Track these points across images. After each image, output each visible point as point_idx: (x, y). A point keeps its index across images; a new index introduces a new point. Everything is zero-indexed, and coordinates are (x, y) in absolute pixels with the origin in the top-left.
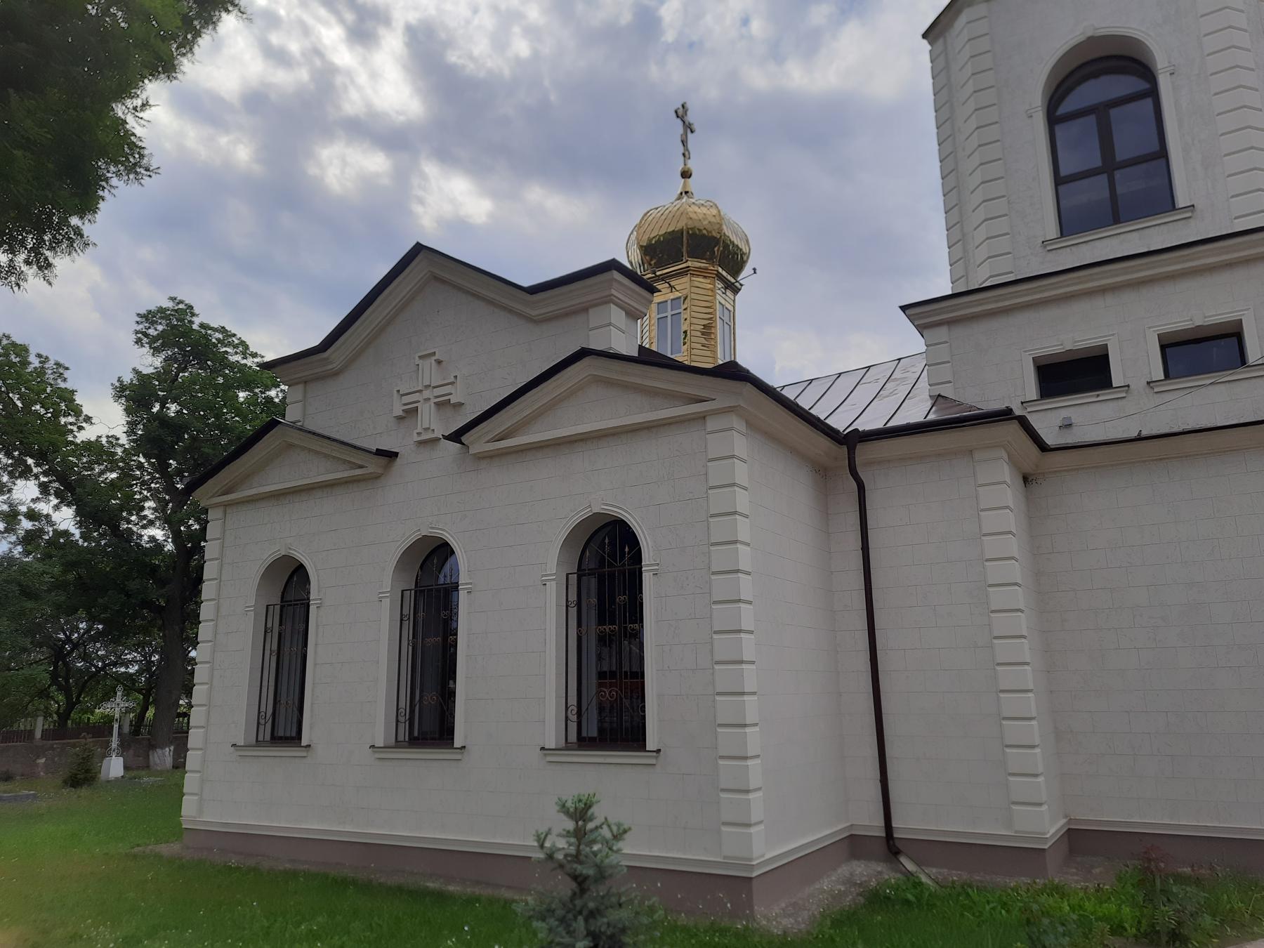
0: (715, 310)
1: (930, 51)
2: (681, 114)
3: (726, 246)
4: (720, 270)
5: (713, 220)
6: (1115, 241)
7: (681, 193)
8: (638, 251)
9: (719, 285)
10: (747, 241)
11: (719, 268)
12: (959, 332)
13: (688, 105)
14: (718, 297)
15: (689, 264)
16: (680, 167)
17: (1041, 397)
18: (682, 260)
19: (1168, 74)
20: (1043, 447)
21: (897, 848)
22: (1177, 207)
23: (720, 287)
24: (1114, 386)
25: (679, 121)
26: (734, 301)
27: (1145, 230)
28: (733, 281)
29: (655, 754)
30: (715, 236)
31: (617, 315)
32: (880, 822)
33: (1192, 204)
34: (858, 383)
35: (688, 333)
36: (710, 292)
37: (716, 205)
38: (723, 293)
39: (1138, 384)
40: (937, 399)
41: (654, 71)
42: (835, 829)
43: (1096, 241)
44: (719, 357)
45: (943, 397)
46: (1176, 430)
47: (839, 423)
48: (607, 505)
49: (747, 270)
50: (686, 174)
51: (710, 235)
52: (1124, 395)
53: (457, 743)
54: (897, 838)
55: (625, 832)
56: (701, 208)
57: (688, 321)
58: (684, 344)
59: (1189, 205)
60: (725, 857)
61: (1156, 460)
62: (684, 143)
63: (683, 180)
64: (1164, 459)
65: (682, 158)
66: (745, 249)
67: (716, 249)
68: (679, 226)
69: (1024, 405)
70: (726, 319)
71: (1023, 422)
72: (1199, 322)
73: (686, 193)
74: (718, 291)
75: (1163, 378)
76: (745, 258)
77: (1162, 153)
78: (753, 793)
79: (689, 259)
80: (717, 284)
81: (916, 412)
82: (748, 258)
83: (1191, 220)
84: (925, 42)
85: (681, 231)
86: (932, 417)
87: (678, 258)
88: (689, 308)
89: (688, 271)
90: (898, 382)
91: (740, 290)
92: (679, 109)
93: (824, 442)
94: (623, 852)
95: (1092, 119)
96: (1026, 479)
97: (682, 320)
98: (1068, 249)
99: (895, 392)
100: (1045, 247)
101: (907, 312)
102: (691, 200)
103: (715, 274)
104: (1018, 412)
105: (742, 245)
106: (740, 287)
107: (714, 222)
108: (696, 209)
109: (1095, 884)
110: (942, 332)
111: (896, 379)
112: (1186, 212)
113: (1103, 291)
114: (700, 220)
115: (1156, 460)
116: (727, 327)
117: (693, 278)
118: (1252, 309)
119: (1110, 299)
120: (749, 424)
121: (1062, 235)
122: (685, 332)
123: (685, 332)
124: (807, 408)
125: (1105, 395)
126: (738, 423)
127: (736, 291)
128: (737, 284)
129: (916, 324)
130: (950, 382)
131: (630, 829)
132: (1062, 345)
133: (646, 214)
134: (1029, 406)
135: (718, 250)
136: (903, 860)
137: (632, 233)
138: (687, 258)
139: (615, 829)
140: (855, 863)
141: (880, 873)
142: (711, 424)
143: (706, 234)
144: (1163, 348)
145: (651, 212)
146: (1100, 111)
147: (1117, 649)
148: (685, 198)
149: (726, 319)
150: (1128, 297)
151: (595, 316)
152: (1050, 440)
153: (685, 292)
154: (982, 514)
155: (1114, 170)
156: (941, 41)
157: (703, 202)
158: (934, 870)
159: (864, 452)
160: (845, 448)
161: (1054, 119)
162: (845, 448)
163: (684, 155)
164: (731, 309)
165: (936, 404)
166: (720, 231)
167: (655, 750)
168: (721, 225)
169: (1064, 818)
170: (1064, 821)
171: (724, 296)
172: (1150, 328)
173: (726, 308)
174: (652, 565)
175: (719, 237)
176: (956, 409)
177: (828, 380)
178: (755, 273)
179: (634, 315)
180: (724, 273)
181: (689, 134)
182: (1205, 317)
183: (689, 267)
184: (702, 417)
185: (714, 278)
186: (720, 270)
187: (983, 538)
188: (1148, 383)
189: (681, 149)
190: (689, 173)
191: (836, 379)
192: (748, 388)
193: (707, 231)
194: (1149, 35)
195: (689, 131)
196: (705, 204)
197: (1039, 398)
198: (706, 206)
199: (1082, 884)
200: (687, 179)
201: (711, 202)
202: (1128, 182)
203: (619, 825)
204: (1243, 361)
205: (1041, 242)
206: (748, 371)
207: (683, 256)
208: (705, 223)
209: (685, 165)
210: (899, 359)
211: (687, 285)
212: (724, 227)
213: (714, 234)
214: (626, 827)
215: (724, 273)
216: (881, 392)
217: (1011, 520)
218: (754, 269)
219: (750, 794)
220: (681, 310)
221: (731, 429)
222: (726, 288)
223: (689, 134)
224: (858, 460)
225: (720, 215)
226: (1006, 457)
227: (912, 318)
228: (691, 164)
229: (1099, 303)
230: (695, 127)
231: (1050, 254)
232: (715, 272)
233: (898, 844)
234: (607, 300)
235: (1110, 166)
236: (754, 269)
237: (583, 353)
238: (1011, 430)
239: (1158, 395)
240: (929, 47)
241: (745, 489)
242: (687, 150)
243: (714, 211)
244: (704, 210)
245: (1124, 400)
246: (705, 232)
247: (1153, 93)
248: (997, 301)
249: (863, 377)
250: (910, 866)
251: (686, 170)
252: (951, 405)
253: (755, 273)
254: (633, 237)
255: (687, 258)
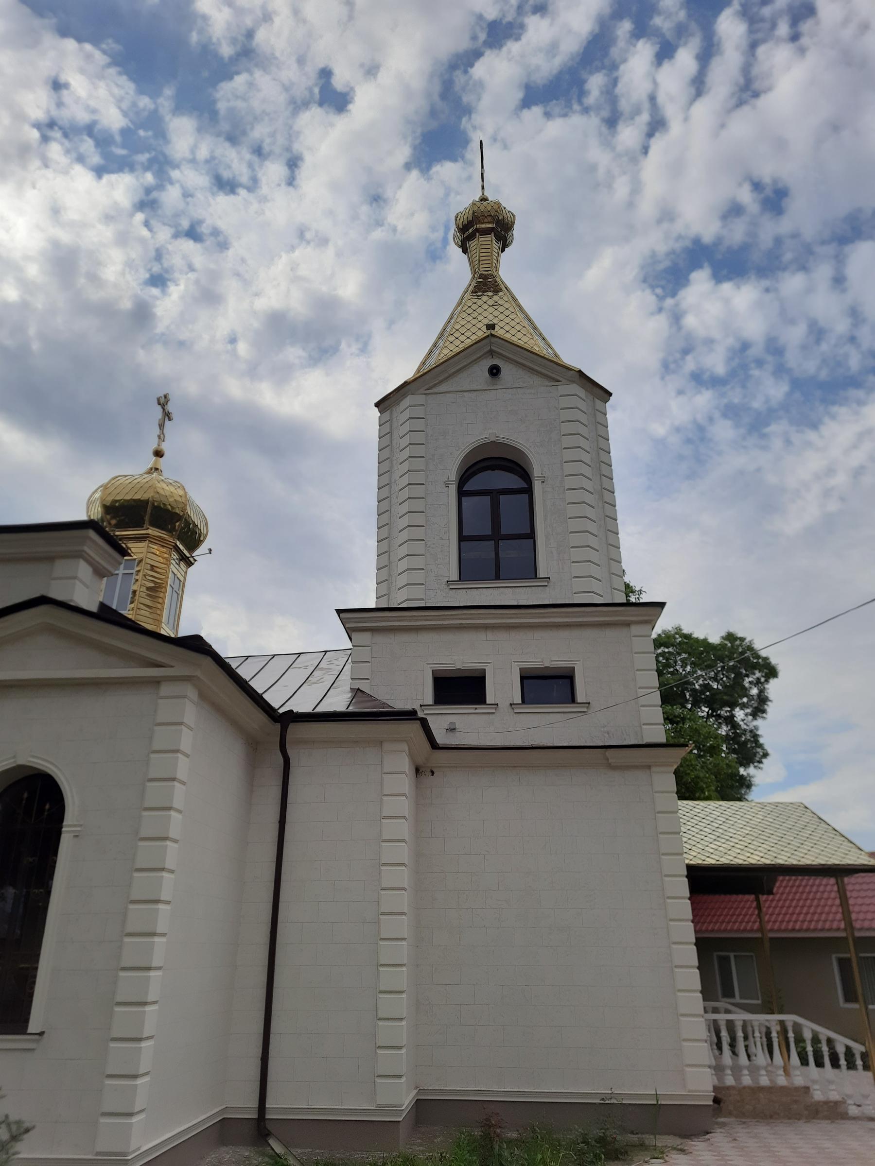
0: (168, 578)
1: (379, 417)
2: (163, 402)
3: (187, 523)
4: (178, 543)
5: (179, 499)
6: (496, 592)
7: (151, 469)
8: (99, 509)
9: (175, 556)
10: (207, 524)
11: (177, 541)
12: (381, 640)
13: (170, 397)
14: (172, 566)
15: (149, 531)
16: (154, 446)
17: (435, 703)
18: (143, 527)
19: (541, 481)
20: (434, 745)
21: (268, 1130)
22: (538, 577)
23: (175, 558)
24: (488, 702)
25: (159, 407)
26: (186, 573)
27: (516, 588)
28: (188, 555)
29: (37, 1037)
30: (178, 512)
31: (84, 570)
32: (255, 1104)
33: (548, 577)
34: (290, 667)
35: (137, 593)
36: (165, 560)
37: (183, 487)
38: (178, 564)
39: (504, 704)
40: (357, 692)
41: (141, 355)
42: (208, 1115)
43: (484, 589)
44: (163, 621)
45: (361, 691)
46: (526, 744)
47: (275, 699)
48: (33, 757)
49: (202, 549)
50: (158, 454)
51: (174, 511)
52: (493, 711)
53: (33, 1027)
54: (268, 1119)
55: (27, 1131)
56: (161, 483)
57: (139, 583)
58: (132, 603)
59: (546, 577)
60: (99, 1154)
61: (512, 767)
62: (161, 426)
63: (154, 458)
64: (518, 767)
65: (157, 439)
66: (204, 530)
67: (177, 524)
68: (146, 497)
69: (423, 707)
70: (176, 587)
71: (424, 723)
72: (547, 664)
73: (157, 469)
74: (173, 561)
75: (521, 702)
76: (202, 539)
77: (531, 536)
78: (141, 1078)
79: (150, 527)
80: (173, 556)
81: (338, 702)
82: (205, 538)
83: (547, 588)
84: (376, 409)
85: (147, 502)
86: (351, 709)
87: (139, 525)
88: (142, 571)
89: (148, 537)
90: (324, 672)
91: (193, 564)
92: (161, 397)
93: (260, 717)
94: (21, 1156)
95: (487, 499)
96: (417, 770)
97: (133, 581)
98: (464, 590)
99: (321, 680)
100: (448, 586)
101: (342, 615)
102: (160, 477)
103: (173, 546)
104: (420, 714)
105: (201, 526)
106: (193, 562)
107: (179, 501)
108: (164, 486)
109: (438, 1153)
110: (364, 638)
111: (322, 669)
112: (543, 581)
113: (486, 627)
114: (166, 496)
115: (512, 767)
116: (175, 595)
117: (150, 545)
118: (582, 661)
119: (490, 635)
120: (202, 696)
121: (460, 580)
122: (134, 592)
123: (134, 592)
124: (260, 691)
125: (481, 709)
126: (191, 692)
127: (189, 564)
128: (191, 559)
129: (347, 625)
130: (368, 679)
131: (34, 1127)
132: (453, 664)
133: (114, 479)
134: (426, 709)
135: (179, 526)
136: (272, 1142)
137: (96, 491)
138: (149, 527)
139: (14, 1128)
140: (224, 1149)
141: (247, 1158)
142: (165, 689)
143: (170, 509)
144: (523, 678)
145: (119, 478)
146: (494, 494)
147: (471, 927)
148: (155, 475)
149: (176, 587)
150: (502, 636)
151: (61, 567)
152: (441, 738)
153: (141, 556)
154: (385, 798)
155: (500, 540)
156: (388, 413)
157: (171, 482)
158: (299, 1151)
159: (295, 731)
160: (278, 725)
161: (462, 493)
162: (278, 725)
163: (159, 437)
164: (182, 579)
165: (355, 697)
166: (184, 510)
167: (38, 1032)
168: (186, 505)
169: (415, 1089)
170: (416, 1091)
171: (177, 566)
172: (515, 662)
173: (178, 578)
174: (75, 826)
175: (181, 515)
176: (369, 704)
177: (264, 659)
178: (210, 553)
179: (100, 573)
180: (181, 547)
181: (167, 421)
182: (552, 661)
183: (148, 534)
184: (156, 682)
185: (171, 549)
186: (178, 543)
187: (382, 820)
188: (511, 705)
189: (157, 431)
190: (162, 454)
191: (270, 660)
192: (208, 661)
193: (171, 507)
194: (531, 452)
195: (167, 418)
196: (173, 484)
197: (433, 704)
198: (174, 486)
199: (427, 1154)
200: (158, 458)
201: (179, 483)
202: (510, 551)
203: (19, 1123)
204: (573, 700)
205: (446, 581)
206: (210, 646)
207: (144, 523)
208: (171, 500)
209: (159, 445)
210: (326, 652)
211: (144, 550)
212: (188, 508)
213: (177, 511)
214: (27, 1125)
215: (181, 547)
216: (310, 679)
217: (404, 806)
218: (210, 550)
219: (138, 1079)
220: (133, 571)
221: (185, 697)
222: (181, 560)
223: (167, 421)
224: (289, 737)
225: (186, 496)
226: (407, 748)
227: (344, 621)
228: (165, 447)
229: (481, 636)
230: (173, 416)
231: (452, 592)
232: (173, 544)
233: (270, 1126)
234: (79, 555)
235: (496, 536)
236: (210, 550)
237: (42, 601)
238: (415, 728)
239: (517, 715)
240: (379, 414)
241: (187, 756)
242: (163, 433)
243: (181, 492)
244: (172, 489)
245: (494, 715)
246: (169, 507)
247: (529, 491)
248: (410, 621)
249: (294, 662)
250: (278, 1149)
251: (159, 450)
252: (367, 699)
253: (210, 553)
254: (97, 495)
255: (149, 527)
